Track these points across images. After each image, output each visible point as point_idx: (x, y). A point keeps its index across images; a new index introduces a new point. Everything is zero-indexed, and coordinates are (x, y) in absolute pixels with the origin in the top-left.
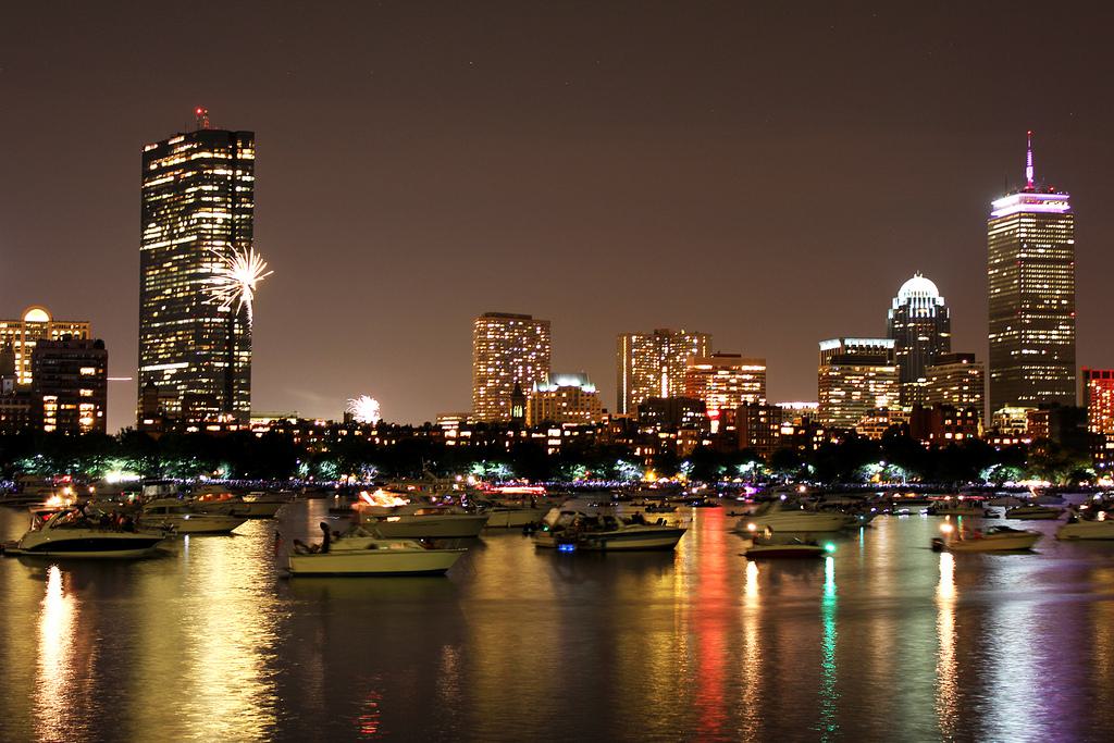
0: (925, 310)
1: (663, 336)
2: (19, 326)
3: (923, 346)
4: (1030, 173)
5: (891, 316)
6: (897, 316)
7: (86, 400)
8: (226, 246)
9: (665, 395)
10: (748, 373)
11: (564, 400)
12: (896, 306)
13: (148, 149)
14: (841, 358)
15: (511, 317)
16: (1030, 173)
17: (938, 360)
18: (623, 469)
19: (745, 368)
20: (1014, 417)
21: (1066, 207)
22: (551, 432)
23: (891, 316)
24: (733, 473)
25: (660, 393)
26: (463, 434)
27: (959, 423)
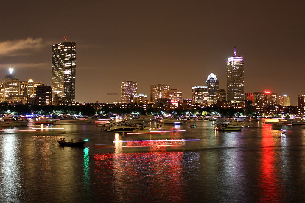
0: (214, 80)
1: (160, 86)
2: (27, 83)
3: (213, 89)
4: (235, 53)
5: (207, 82)
6: (208, 82)
7: (48, 98)
8: (70, 66)
9: (160, 98)
10: (178, 93)
11: (140, 99)
12: (207, 80)
13: (53, 46)
14: (197, 90)
15: (250, 94)
16: (235, 53)
17: (217, 91)
18: (162, 113)
19: (177, 92)
20: (232, 102)
21: (242, 60)
22: (144, 105)
23: (207, 82)
24: (185, 114)
25: (159, 97)
26: (126, 106)
27: (227, 104)
